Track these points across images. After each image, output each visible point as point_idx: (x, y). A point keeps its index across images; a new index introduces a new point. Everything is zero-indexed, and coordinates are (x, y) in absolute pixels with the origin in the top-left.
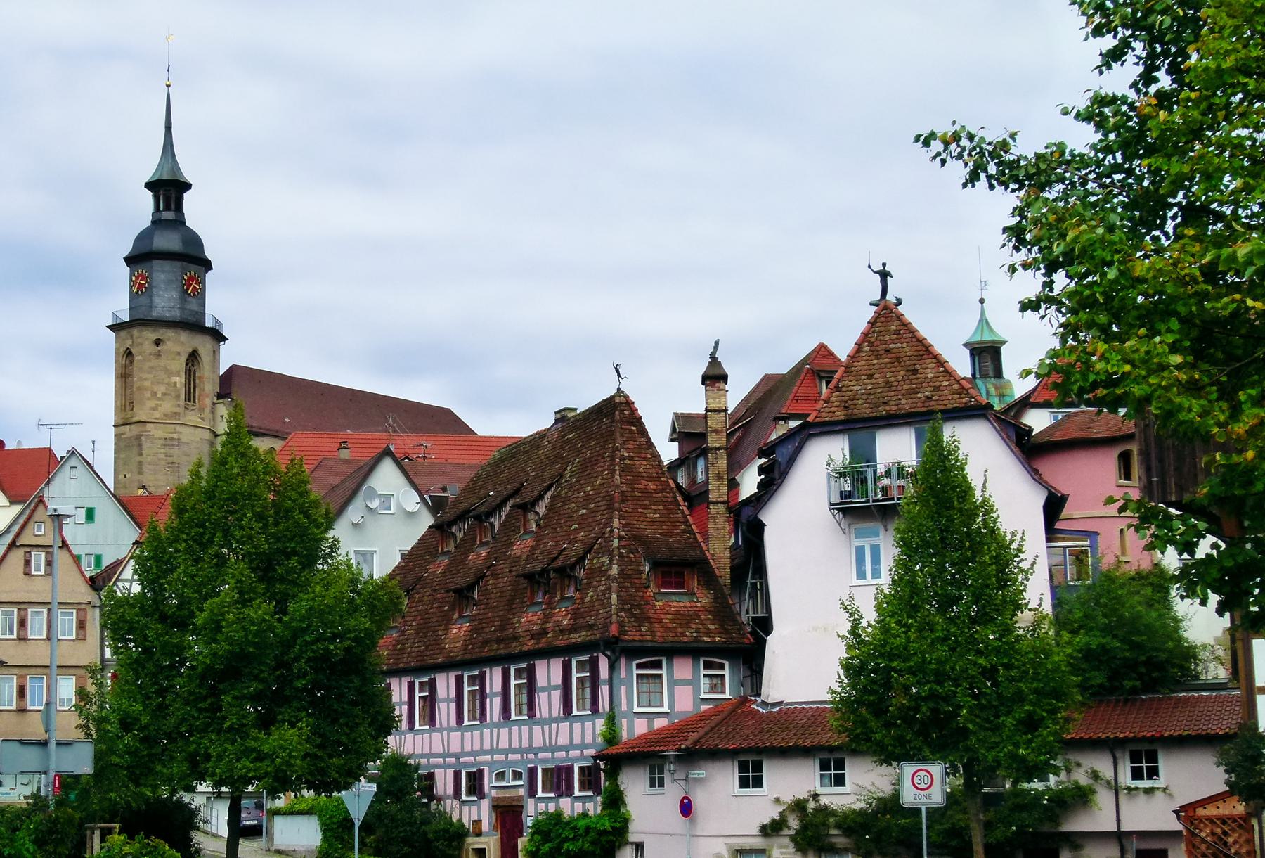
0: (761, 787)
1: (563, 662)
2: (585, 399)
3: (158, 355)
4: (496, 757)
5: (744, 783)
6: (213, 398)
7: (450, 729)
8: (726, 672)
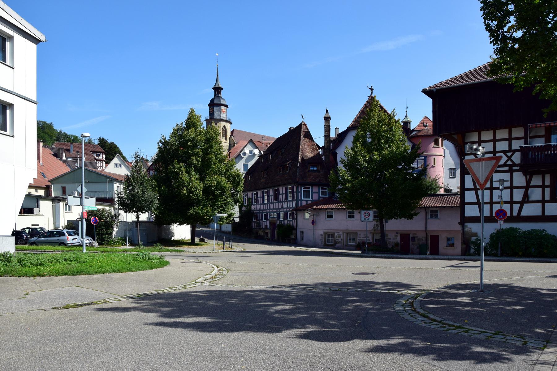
0: (333, 218)
1: (286, 187)
2: (295, 125)
4: (271, 211)
5: (349, 217)
7: (261, 204)
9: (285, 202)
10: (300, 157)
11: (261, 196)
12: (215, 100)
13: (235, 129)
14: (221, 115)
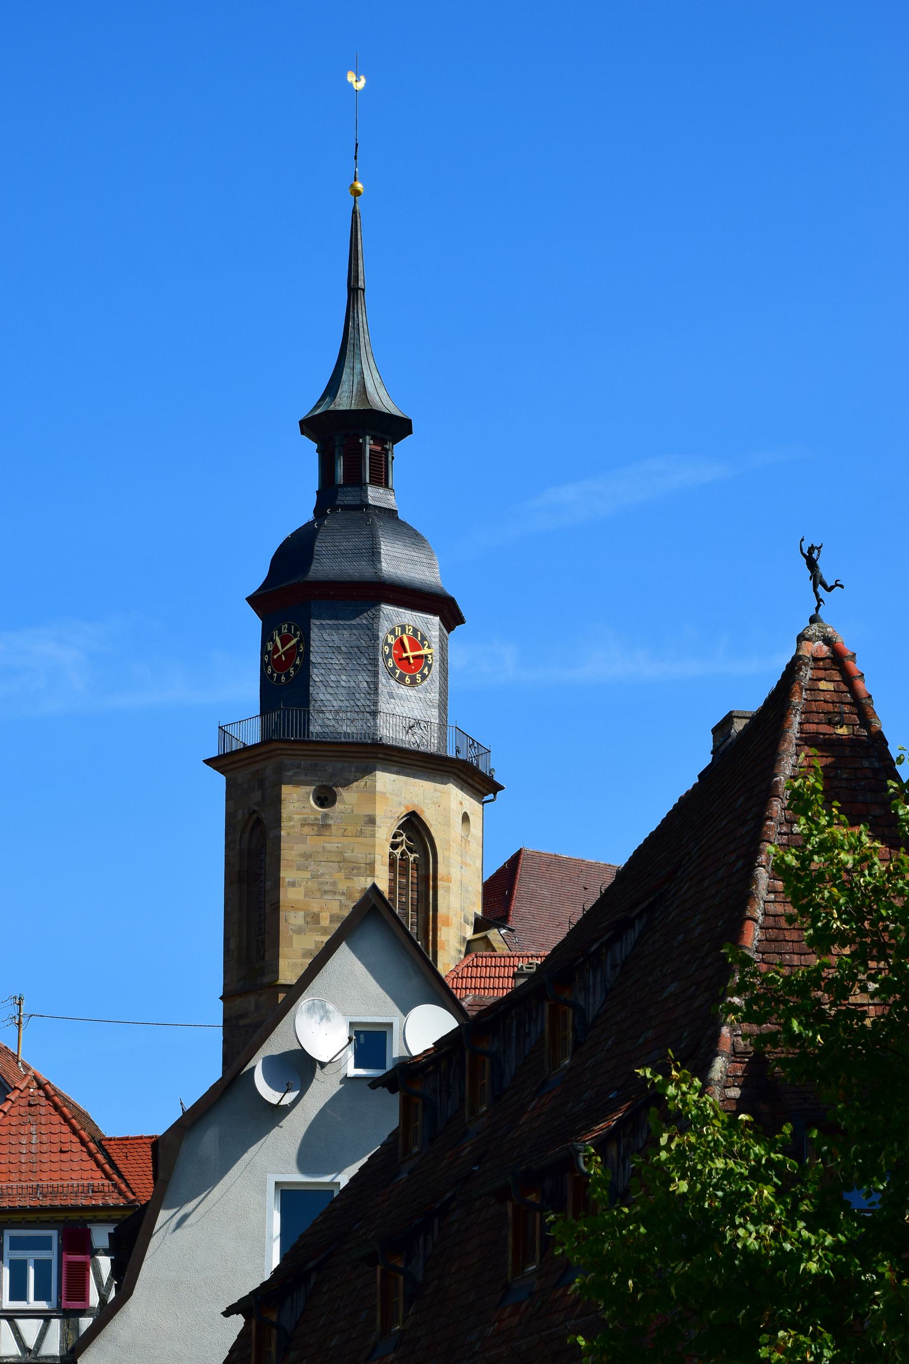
3: (323, 827)
10: (735, 1054)
12: (319, 546)
13: (530, 847)
14: (383, 706)
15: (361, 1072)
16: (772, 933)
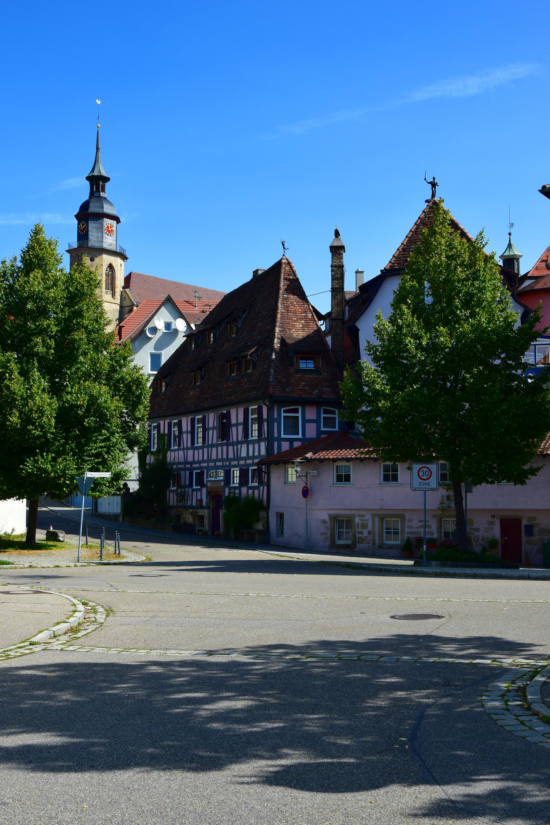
6: (120, 289)
8: (337, 416)
9: (242, 443)
11: (189, 429)
13: (133, 272)
15: (166, 331)
16: (282, 316)
